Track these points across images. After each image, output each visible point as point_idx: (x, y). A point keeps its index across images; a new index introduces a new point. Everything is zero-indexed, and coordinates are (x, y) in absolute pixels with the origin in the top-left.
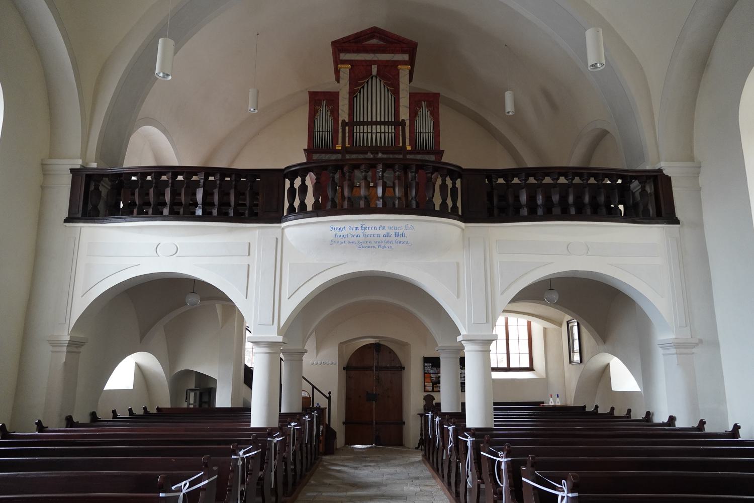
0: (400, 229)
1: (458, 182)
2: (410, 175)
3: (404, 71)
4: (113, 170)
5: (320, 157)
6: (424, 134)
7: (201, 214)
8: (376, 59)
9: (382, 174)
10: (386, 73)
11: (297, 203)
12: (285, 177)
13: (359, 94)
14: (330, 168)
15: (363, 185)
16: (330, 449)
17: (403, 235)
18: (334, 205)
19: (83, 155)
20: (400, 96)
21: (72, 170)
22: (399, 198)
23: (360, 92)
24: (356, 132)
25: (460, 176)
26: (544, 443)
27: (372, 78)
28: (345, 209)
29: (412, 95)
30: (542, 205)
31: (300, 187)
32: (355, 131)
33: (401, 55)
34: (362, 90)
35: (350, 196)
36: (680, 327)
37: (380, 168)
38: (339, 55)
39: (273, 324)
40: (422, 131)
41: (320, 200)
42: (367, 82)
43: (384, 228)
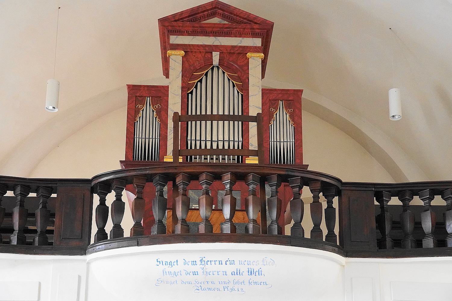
0: (254, 263)
1: (336, 200)
2: (268, 189)
11: (109, 227)
12: (93, 190)
13: (195, 89)
14: (158, 178)
15: (203, 201)
17: (260, 273)
18: (162, 229)
22: (254, 221)
23: (196, 87)
25: (339, 193)
26: (136, 157)
27: (212, 69)
28: (178, 235)
29: (266, 92)
31: (114, 204)
32: (189, 138)
34: (199, 83)
35: (184, 218)
37: (227, 178)
38: (168, 38)
41: (142, 222)
42: (206, 75)
43: (232, 263)
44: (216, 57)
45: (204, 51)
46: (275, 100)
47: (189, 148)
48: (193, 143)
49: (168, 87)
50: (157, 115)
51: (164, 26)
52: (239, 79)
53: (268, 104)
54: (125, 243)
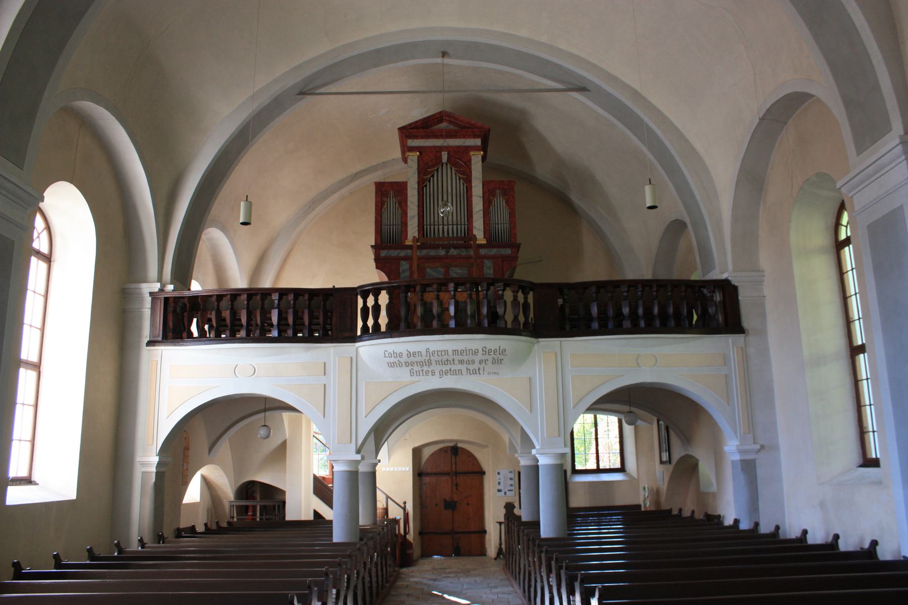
3: (476, 160)
5: (389, 253)
6: (500, 225)
7: (277, 336)
8: (446, 144)
9: (454, 293)
10: (458, 160)
11: (370, 322)
13: (428, 184)
16: (406, 560)
23: (429, 181)
25: (532, 289)
27: (442, 165)
38: (406, 141)
42: (437, 170)
44: (445, 156)
48: (428, 227)
50: (399, 205)
52: (463, 173)
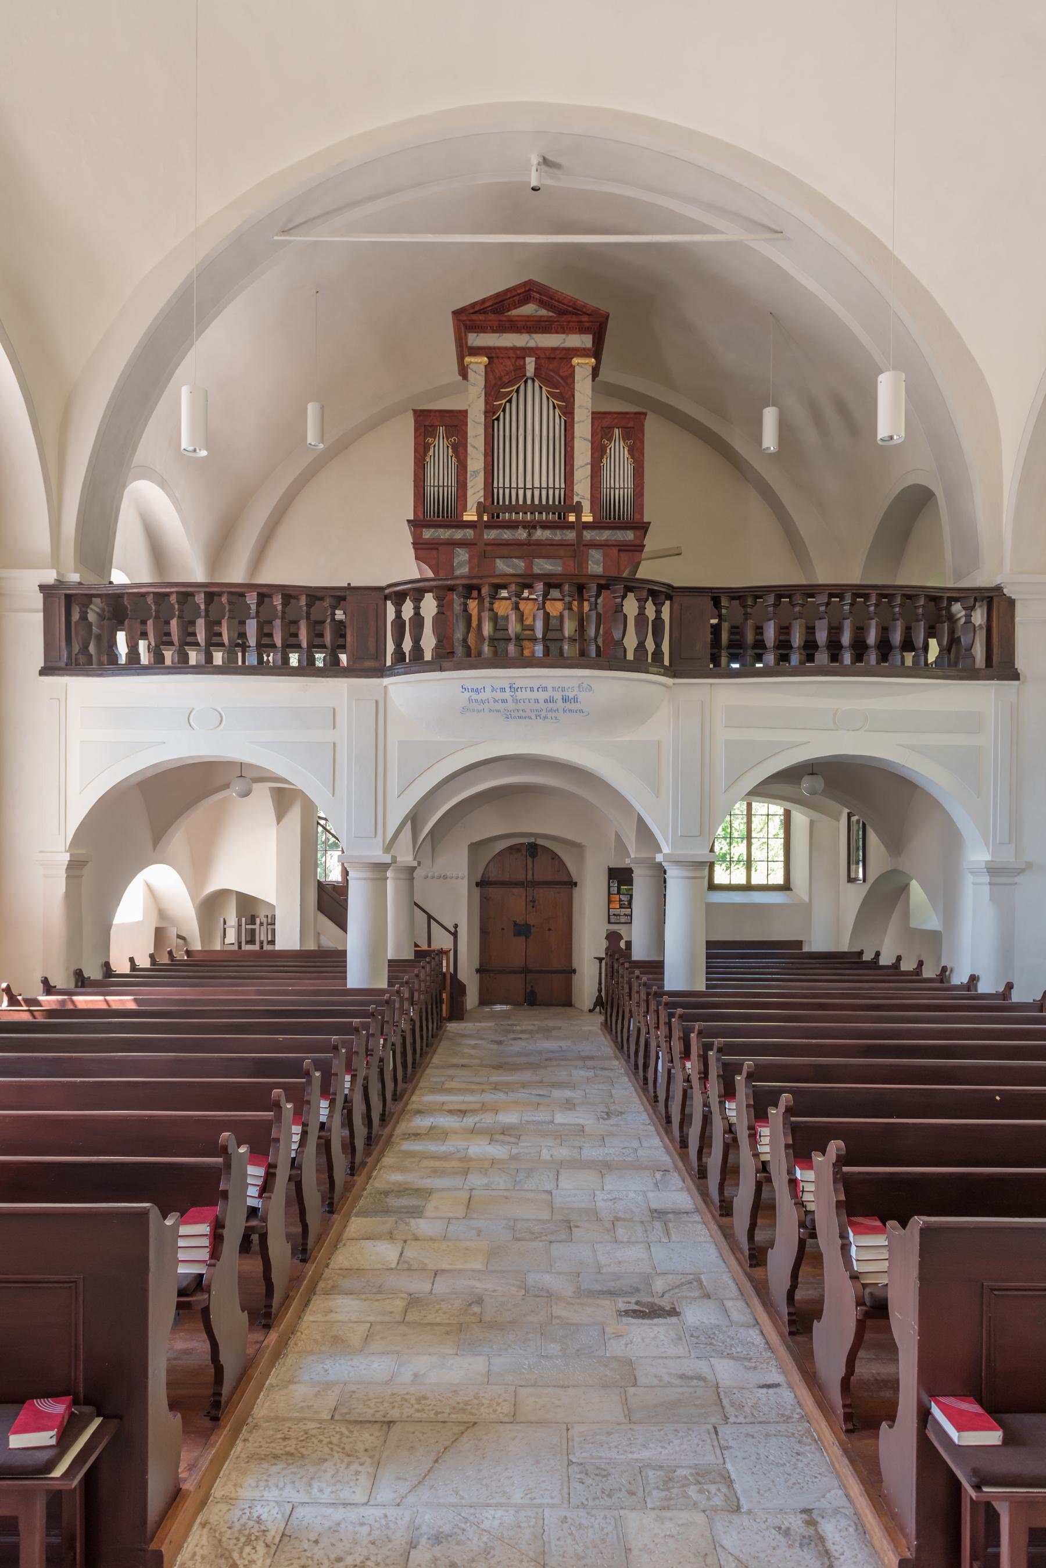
0: (570, 690)
3: (582, 366)
4: (109, 589)
7: (256, 663)
11: (407, 645)
13: (502, 414)
16: (457, 1013)
17: (575, 700)
19: (55, 561)
20: (576, 419)
21: (42, 588)
23: (504, 411)
24: (498, 488)
25: (669, 597)
27: (526, 382)
29: (596, 416)
30: (799, 648)
32: (495, 485)
33: (578, 336)
34: (508, 405)
36: (999, 844)
38: (466, 335)
39: (375, 837)
40: (612, 486)
42: (517, 391)
43: (545, 689)
45: (514, 356)
46: (609, 428)
47: (495, 504)
49: (466, 412)
50: (453, 452)
51: (459, 320)
52: (560, 397)
53: (600, 435)
54: (427, 667)
